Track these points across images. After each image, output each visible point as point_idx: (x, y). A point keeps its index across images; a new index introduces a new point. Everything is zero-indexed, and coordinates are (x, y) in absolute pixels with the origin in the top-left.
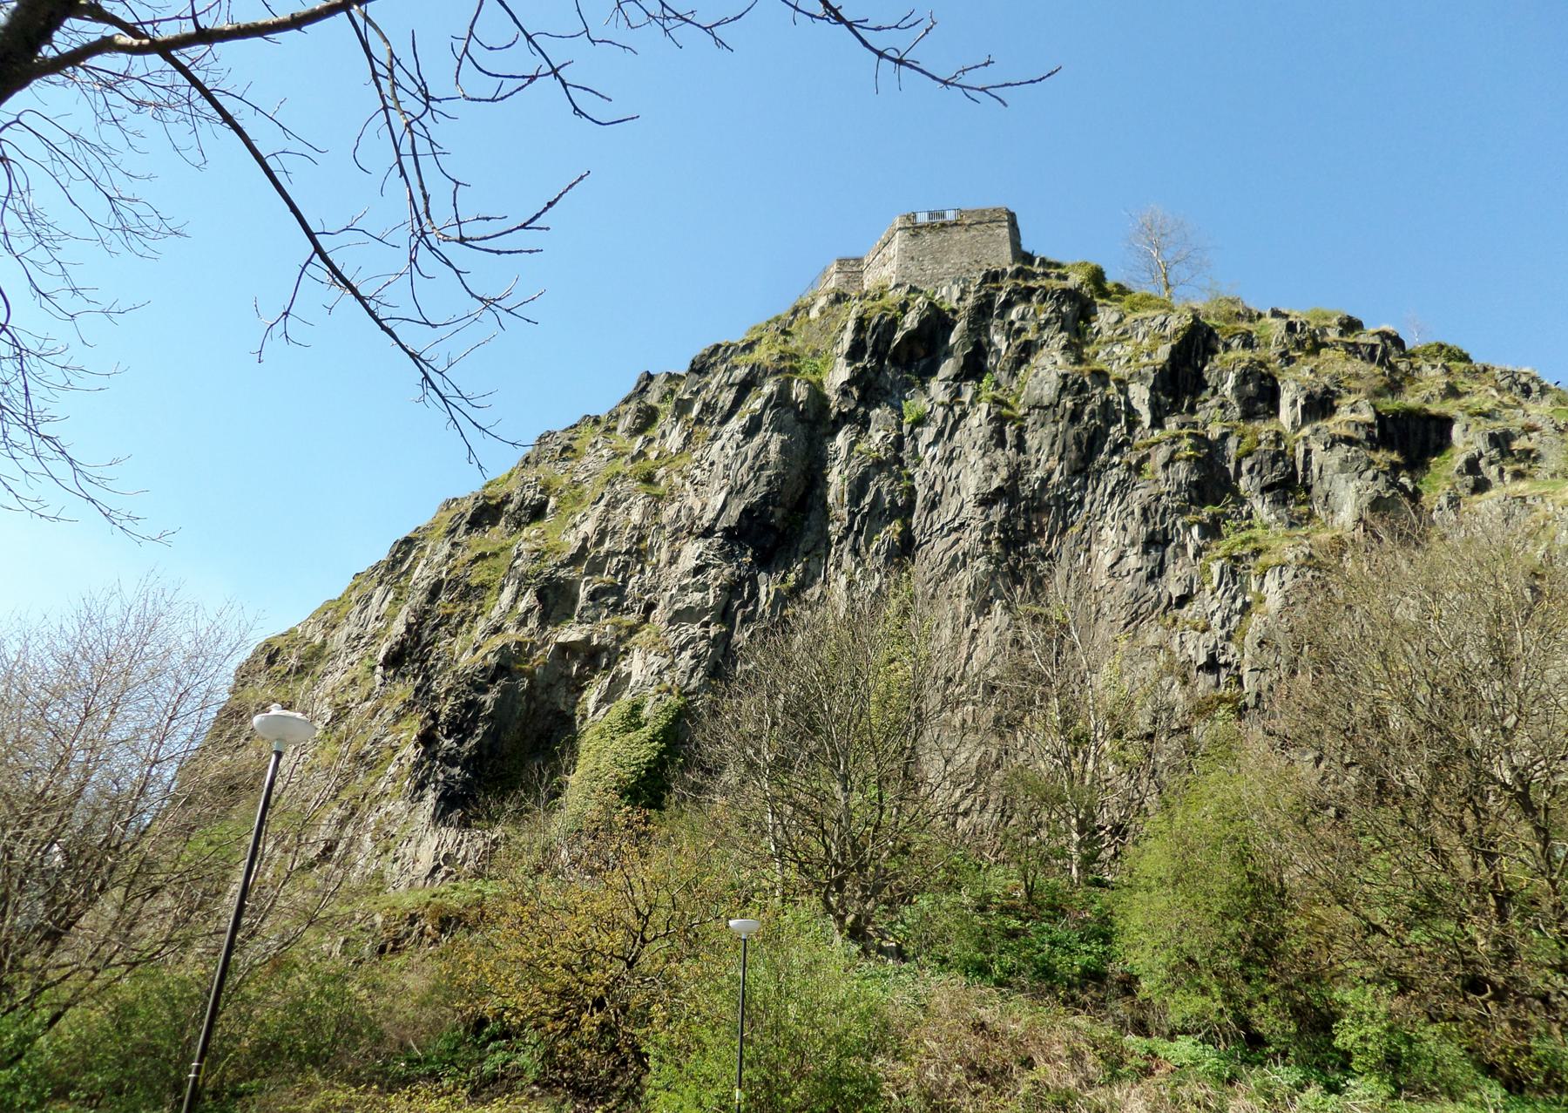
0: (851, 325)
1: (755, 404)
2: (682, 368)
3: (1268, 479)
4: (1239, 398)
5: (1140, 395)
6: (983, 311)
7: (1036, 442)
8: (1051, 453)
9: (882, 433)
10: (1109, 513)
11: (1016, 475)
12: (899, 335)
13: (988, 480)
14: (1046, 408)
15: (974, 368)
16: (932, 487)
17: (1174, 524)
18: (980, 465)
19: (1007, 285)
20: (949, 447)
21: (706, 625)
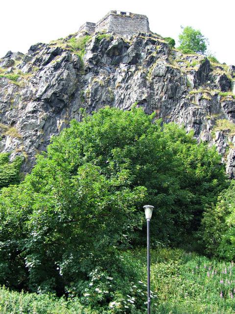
0: (94, 40)
1: (59, 59)
2: (25, 51)
3: (230, 110)
4: (220, 85)
5: (191, 78)
6: (139, 43)
7: (157, 87)
8: (162, 91)
9: (103, 77)
10: (181, 114)
11: (151, 96)
12: (110, 47)
13: (141, 96)
14: (161, 77)
15: (135, 61)
16: (120, 96)
17: (203, 118)
18: (138, 91)
19: (146, 38)
20: (127, 84)
21: (37, 131)
